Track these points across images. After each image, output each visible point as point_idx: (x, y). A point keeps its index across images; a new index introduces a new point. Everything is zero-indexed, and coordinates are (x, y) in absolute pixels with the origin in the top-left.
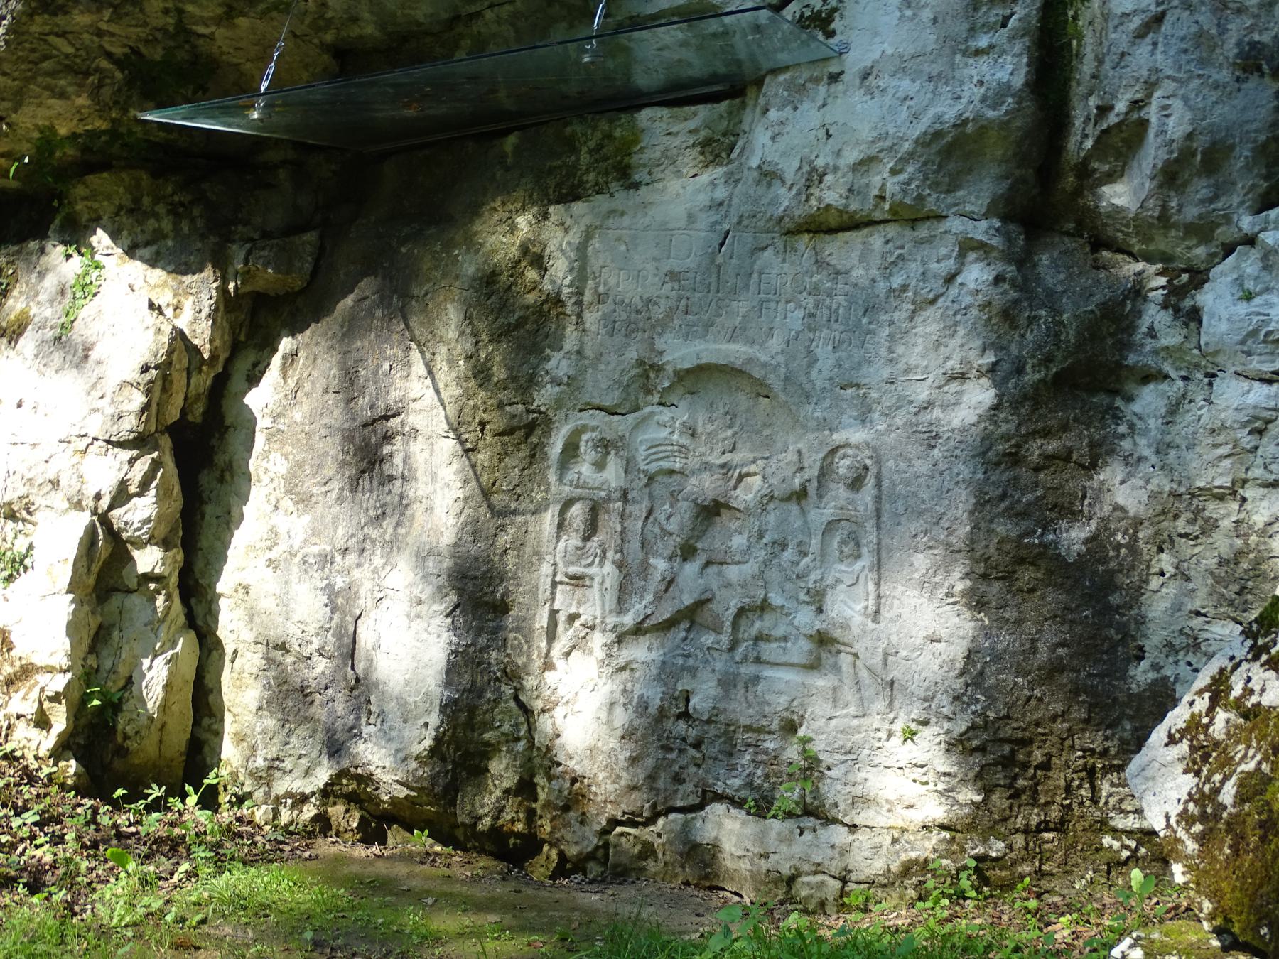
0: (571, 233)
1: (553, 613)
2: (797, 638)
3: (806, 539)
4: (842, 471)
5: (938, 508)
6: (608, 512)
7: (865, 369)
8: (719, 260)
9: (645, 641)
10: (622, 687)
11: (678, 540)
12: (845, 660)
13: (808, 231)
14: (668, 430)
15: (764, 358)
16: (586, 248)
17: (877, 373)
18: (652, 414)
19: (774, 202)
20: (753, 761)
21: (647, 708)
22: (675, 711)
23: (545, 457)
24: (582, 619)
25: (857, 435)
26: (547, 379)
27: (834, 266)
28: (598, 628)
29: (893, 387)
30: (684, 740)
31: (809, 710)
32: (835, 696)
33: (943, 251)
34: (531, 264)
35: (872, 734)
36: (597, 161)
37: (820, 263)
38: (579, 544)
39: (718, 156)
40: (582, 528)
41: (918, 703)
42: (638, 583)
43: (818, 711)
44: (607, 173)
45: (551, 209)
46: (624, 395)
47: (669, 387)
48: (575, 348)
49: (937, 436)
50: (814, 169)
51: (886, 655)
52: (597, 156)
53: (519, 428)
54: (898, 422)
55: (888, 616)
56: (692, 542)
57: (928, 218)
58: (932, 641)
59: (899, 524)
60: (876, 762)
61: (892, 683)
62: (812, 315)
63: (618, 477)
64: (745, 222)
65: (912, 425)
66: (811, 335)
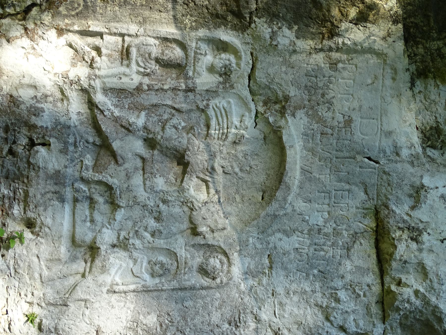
0: (382, 42)
1: (101, 35)
2: (93, 231)
3: (163, 236)
4: (212, 260)
5: (188, 330)
6: (178, 78)
7: (282, 273)
8: (359, 158)
9: (84, 109)
10: (49, 93)
11: (159, 137)
12: (80, 266)
13: (377, 226)
14: (238, 124)
15: (290, 198)
16: (370, 53)
17: (280, 281)
18: (250, 111)
19: (398, 201)
20: (4, 196)
21: (35, 115)
22: (35, 137)
23: (217, 26)
24: (97, 59)
25: (236, 271)
26: (275, 29)
27: (353, 247)
28: (92, 72)
29: (270, 295)
30: (14, 142)
31: (43, 241)
32: (54, 260)
33: (361, 323)
34: (360, 12)
35: (29, 290)
36: (432, 54)
37: (355, 236)
38: (153, 56)
39: (429, 139)
40: (165, 58)
41: (53, 324)
42: (127, 102)
43: (43, 247)
44: (422, 62)
45: (400, 26)
46: (263, 86)
47: (269, 123)
48: (298, 49)
49: (237, 327)
50: (420, 233)
51: (86, 301)
52: (435, 55)
53: (238, 6)
54: (247, 299)
55: (113, 299)
56: (158, 147)
57: (384, 311)
58: (97, 331)
59: (176, 303)
60: (11, 292)
61: (66, 305)
62: (319, 231)
63: (203, 84)
64: (385, 177)
65: (244, 309)
66: (306, 232)
